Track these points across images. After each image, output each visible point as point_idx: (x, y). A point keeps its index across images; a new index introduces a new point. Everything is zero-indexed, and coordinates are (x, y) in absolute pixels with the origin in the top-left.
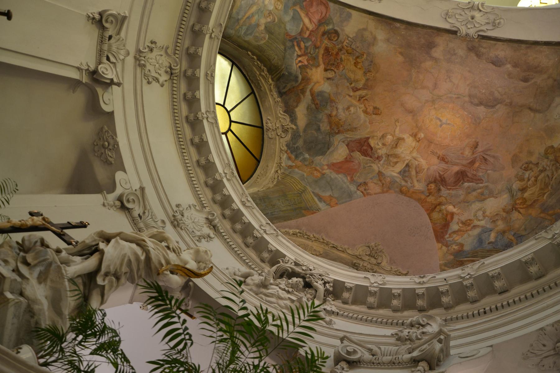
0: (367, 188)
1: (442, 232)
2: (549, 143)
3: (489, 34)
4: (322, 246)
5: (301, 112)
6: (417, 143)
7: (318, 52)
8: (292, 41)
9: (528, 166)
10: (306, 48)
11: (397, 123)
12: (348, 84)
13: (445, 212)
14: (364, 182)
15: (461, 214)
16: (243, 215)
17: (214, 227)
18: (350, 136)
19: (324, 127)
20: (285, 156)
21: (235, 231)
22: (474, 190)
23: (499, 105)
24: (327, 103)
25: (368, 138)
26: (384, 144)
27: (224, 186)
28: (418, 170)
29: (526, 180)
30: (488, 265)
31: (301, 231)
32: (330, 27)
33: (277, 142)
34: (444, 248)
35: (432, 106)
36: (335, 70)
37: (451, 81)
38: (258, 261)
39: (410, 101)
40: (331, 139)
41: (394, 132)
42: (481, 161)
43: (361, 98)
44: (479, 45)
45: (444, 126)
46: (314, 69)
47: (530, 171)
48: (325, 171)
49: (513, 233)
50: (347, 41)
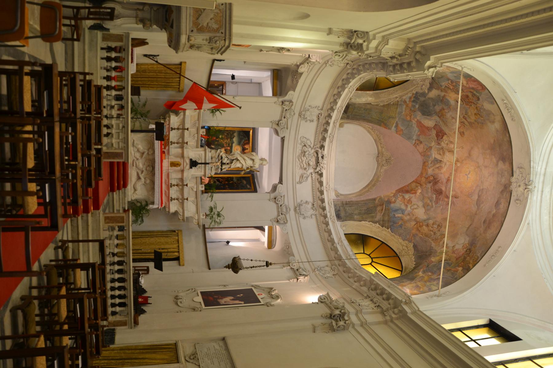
15: (415, 199)
19: (438, 108)
20: (410, 95)
22: (431, 201)
26: (447, 144)
39: (476, 152)
44: (506, 191)
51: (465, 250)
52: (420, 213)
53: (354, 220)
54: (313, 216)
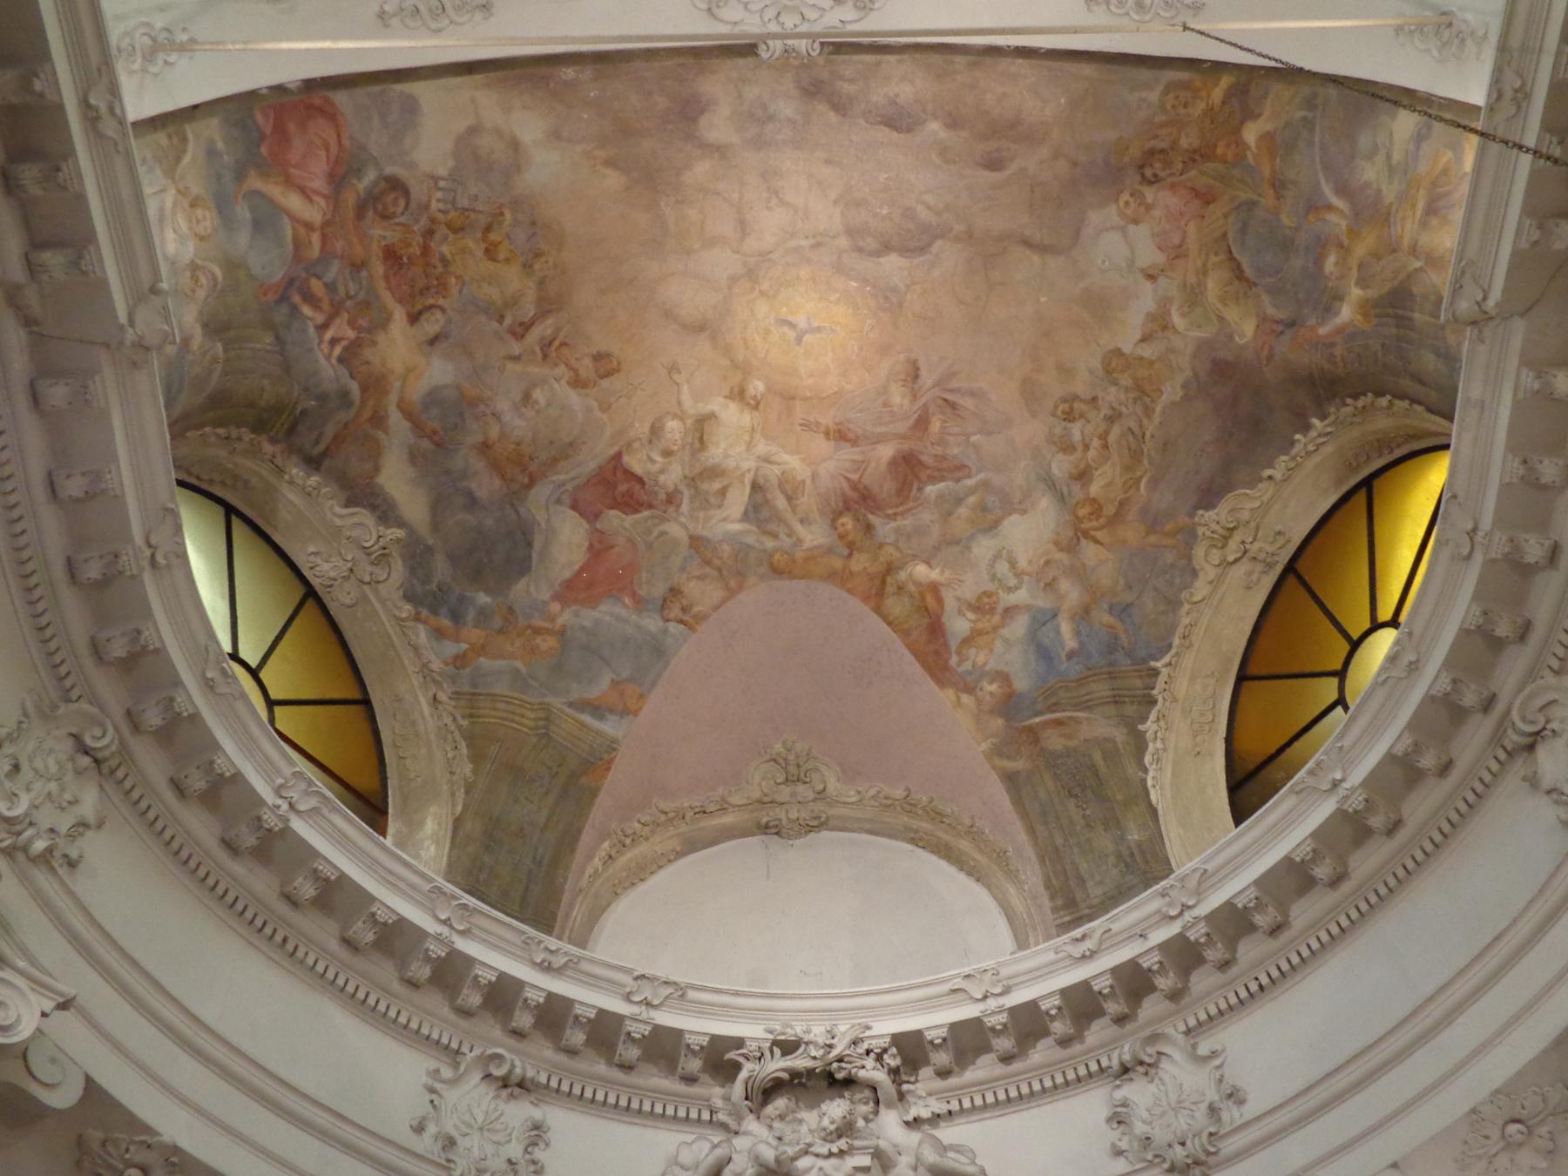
0: (685, 602)
1: (937, 653)
5: (397, 479)
6: (755, 413)
9: (1072, 409)
10: (331, 287)
11: (676, 377)
12: (495, 325)
13: (911, 588)
15: (960, 585)
17: (521, 1085)
18: (570, 474)
19: (486, 485)
20: (422, 635)
21: (572, 1052)
22: (959, 501)
23: (939, 243)
24: (461, 414)
25: (618, 456)
26: (667, 453)
27: (470, 961)
28: (788, 487)
32: (370, 176)
33: (378, 606)
35: (753, 289)
36: (441, 302)
38: (681, 1088)
40: (522, 510)
41: (679, 403)
42: (944, 413)
43: (546, 345)
45: (808, 338)
48: (560, 621)
49: (1105, 607)
50: (439, 195)
51: (1149, 194)
52: (1030, 532)
53: (1157, 837)
54: (1203, 1050)
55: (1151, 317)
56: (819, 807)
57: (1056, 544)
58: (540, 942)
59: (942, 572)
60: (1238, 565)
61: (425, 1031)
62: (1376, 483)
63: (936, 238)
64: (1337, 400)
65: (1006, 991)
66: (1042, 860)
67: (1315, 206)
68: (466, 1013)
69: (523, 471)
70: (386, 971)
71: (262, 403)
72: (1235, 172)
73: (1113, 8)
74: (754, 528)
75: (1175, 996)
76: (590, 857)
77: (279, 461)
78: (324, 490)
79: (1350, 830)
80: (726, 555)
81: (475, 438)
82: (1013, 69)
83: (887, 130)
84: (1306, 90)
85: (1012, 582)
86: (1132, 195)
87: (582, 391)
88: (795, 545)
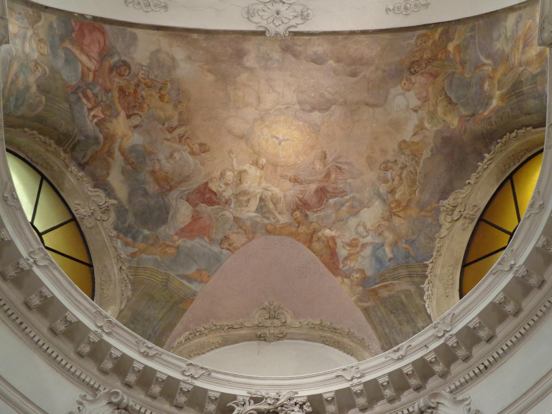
0: (230, 242)
1: (334, 263)
2: (400, 138)
3: (301, 28)
4: (218, 334)
5: (116, 179)
7: (112, 96)
8: (75, 93)
9: (387, 166)
10: (96, 95)
11: (231, 155)
12: (161, 126)
13: (324, 239)
14: (225, 237)
15: (343, 236)
16: (155, 371)
19: (152, 188)
20: (119, 244)
21: (154, 397)
22: (343, 205)
23: (334, 106)
24: (144, 158)
25: (207, 183)
26: (227, 184)
27: (109, 346)
28: (274, 200)
29: (391, 180)
30: (459, 314)
31: (192, 332)
32: (116, 58)
34: (346, 280)
36: (140, 113)
37: (274, 91)
40: (166, 200)
41: (232, 165)
42: (336, 171)
43: (181, 137)
45: (283, 143)
46: (114, 121)
47: (391, 170)
48: (177, 243)
49: (404, 241)
50: (143, 72)
51: (413, 78)
52: (372, 215)
54: (460, 398)
55: (417, 126)
56: (283, 329)
57: (383, 218)
58: (144, 343)
59: (336, 232)
60: (459, 221)
61: (83, 377)
62: (514, 177)
63: (332, 104)
64: (495, 142)
65: (362, 376)
66: (380, 339)
67: (478, 66)
68: (104, 372)
69: (168, 184)
70: (68, 347)
71: (61, 131)
72: (446, 63)
73: (396, 11)
74: (259, 215)
75: (443, 375)
76: (180, 335)
77: (67, 161)
78: (85, 179)
79: (522, 287)
80: (248, 225)
81: (149, 168)
82: (360, 39)
83: (313, 64)
84: (471, 25)
85: (365, 234)
86: (407, 80)
87: (194, 157)
88: (276, 222)
